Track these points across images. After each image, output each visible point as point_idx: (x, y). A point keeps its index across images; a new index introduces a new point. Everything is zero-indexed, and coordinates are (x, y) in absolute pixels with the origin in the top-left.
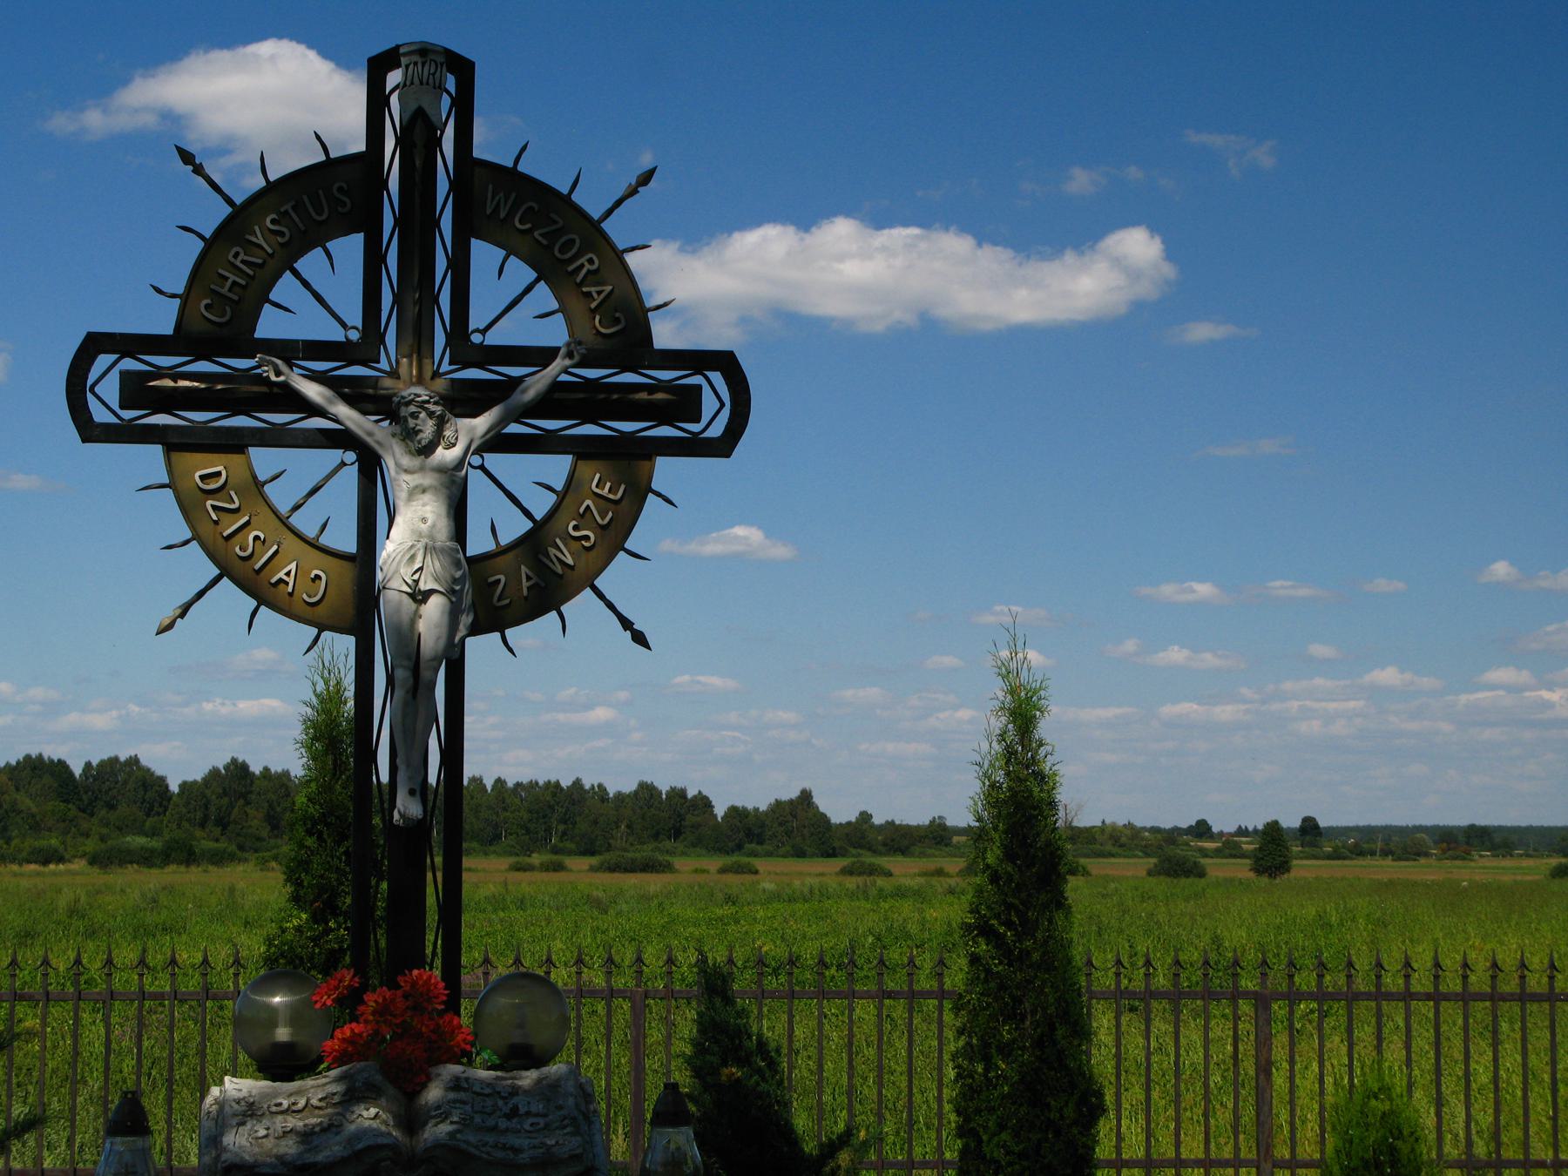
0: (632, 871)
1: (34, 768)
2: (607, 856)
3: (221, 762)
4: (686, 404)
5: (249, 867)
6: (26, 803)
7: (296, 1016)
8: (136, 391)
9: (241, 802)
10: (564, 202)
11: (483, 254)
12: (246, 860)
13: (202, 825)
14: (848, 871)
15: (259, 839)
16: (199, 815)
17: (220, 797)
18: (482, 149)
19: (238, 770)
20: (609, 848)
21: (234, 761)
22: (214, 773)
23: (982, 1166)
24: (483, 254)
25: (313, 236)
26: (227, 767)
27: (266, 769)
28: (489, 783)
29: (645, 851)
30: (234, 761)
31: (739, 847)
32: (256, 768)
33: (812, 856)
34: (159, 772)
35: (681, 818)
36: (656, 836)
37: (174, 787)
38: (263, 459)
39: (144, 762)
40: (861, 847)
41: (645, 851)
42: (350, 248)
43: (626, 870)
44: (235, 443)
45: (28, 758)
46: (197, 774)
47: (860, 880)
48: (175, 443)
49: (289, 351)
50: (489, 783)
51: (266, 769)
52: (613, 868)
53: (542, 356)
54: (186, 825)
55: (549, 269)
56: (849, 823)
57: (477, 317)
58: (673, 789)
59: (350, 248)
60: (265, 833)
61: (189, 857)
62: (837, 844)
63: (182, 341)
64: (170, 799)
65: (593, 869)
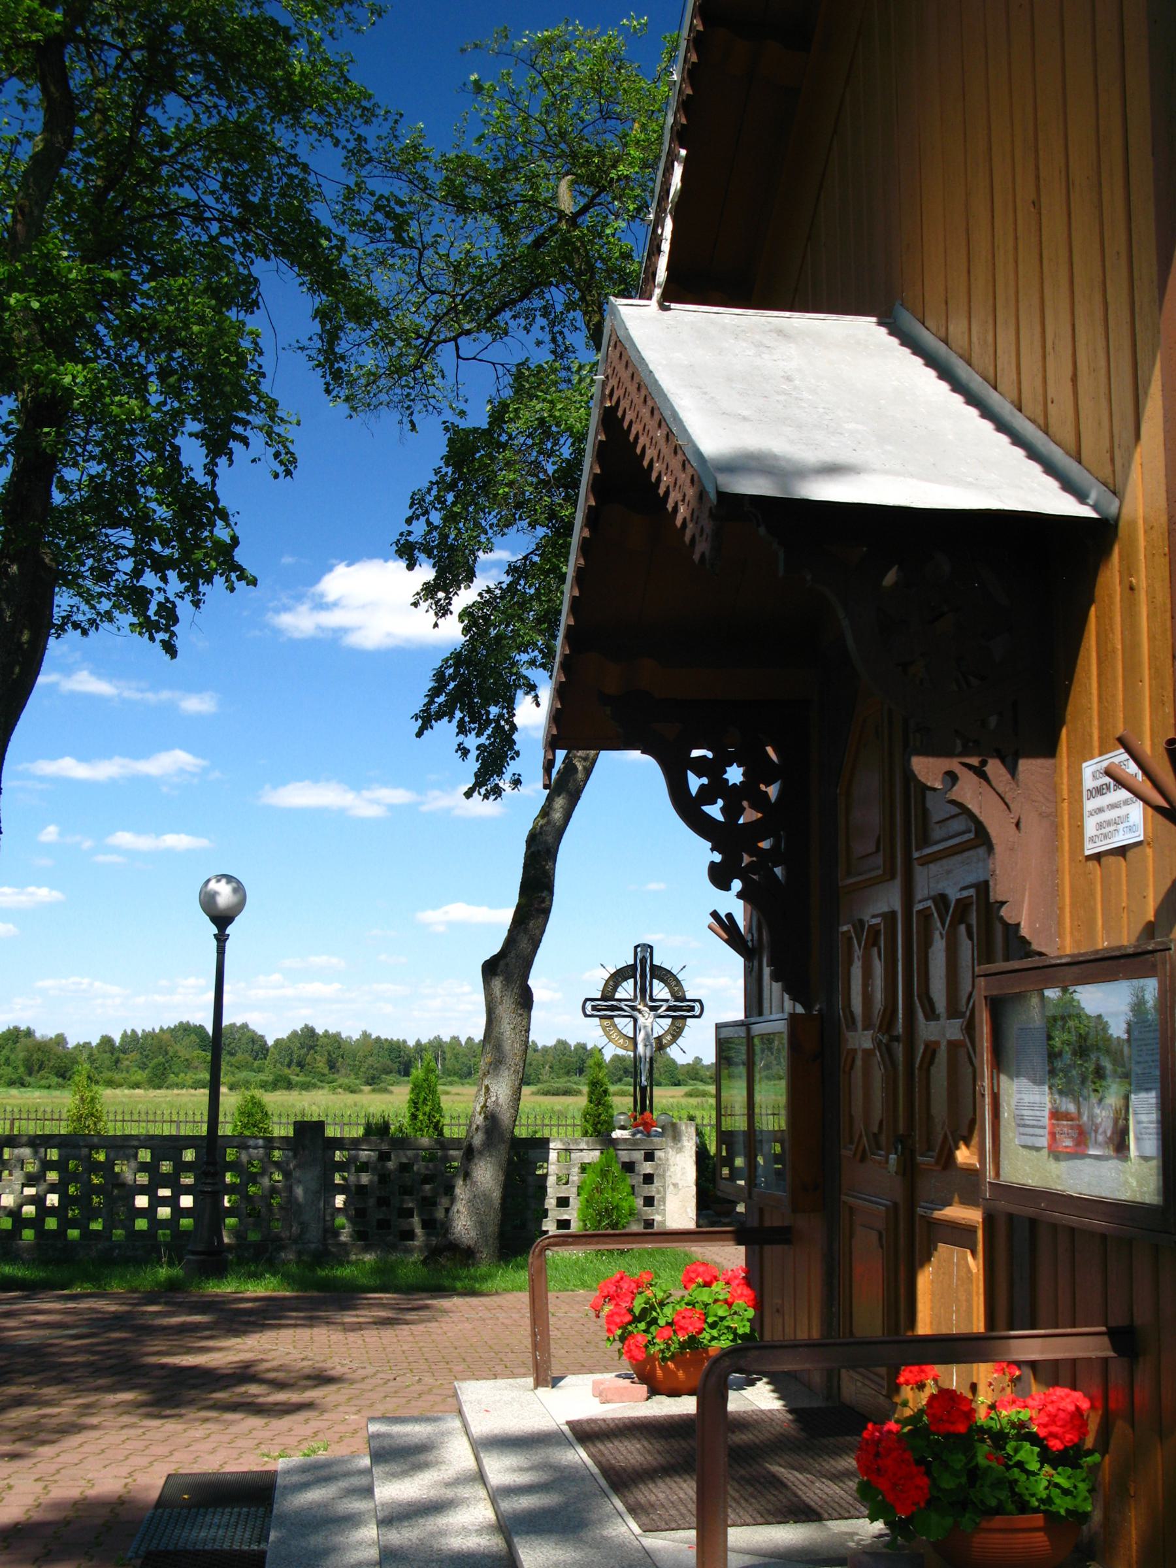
0: (558, 1095)
1: (185, 1030)
2: (540, 1086)
3: (298, 1027)
4: (692, 1009)
5: (325, 1091)
6: (184, 1053)
7: (625, 1120)
8: (594, 1008)
9: (312, 1052)
10: (669, 972)
11: (655, 982)
12: (323, 1088)
13: (289, 1066)
14: (689, 1095)
15: (324, 1075)
16: (287, 1060)
17: (299, 1049)
18: (655, 963)
19: (309, 1032)
20: (539, 1081)
21: (306, 1026)
22: (295, 1033)
23: (567, 202)
24: (655, 982)
25: (626, 979)
26: (302, 1030)
27: (326, 1031)
28: (463, 1041)
29: (561, 1083)
30: (306, 1026)
31: (620, 1080)
32: (320, 1031)
33: (666, 1085)
34: (260, 1033)
35: (583, 1061)
36: (568, 1073)
37: (270, 1042)
38: (616, 1020)
39: (251, 1027)
40: (695, 1079)
41: (561, 1083)
42: (631, 981)
43: (554, 1094)
44: (611, 1017)
45: (181, 1023)
46: (284, 1034)
47: (699, 1100)
48: (601, 1017)
49: (620, 1000)
50: (463, 1041)
51: (326, 1031)
52: (546, 1093)
53: (667, 1001)
54: (278, 1065)
55: (667, 984)
56: (689, 1064)
57: (655, 993)
58: (578, 1044)
59: (631, 981)
60: (326, 1071)
61: (289, 1086)
62: (681, 1078)
63: (603, 998)
64: (267, 1050)
65: (533, 1094)
